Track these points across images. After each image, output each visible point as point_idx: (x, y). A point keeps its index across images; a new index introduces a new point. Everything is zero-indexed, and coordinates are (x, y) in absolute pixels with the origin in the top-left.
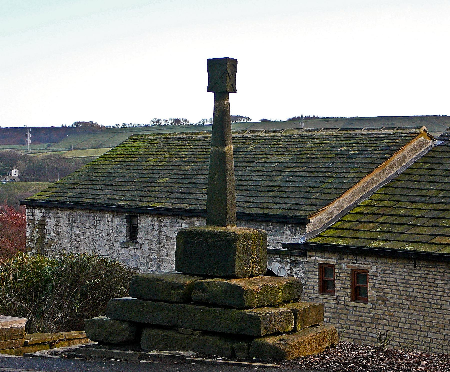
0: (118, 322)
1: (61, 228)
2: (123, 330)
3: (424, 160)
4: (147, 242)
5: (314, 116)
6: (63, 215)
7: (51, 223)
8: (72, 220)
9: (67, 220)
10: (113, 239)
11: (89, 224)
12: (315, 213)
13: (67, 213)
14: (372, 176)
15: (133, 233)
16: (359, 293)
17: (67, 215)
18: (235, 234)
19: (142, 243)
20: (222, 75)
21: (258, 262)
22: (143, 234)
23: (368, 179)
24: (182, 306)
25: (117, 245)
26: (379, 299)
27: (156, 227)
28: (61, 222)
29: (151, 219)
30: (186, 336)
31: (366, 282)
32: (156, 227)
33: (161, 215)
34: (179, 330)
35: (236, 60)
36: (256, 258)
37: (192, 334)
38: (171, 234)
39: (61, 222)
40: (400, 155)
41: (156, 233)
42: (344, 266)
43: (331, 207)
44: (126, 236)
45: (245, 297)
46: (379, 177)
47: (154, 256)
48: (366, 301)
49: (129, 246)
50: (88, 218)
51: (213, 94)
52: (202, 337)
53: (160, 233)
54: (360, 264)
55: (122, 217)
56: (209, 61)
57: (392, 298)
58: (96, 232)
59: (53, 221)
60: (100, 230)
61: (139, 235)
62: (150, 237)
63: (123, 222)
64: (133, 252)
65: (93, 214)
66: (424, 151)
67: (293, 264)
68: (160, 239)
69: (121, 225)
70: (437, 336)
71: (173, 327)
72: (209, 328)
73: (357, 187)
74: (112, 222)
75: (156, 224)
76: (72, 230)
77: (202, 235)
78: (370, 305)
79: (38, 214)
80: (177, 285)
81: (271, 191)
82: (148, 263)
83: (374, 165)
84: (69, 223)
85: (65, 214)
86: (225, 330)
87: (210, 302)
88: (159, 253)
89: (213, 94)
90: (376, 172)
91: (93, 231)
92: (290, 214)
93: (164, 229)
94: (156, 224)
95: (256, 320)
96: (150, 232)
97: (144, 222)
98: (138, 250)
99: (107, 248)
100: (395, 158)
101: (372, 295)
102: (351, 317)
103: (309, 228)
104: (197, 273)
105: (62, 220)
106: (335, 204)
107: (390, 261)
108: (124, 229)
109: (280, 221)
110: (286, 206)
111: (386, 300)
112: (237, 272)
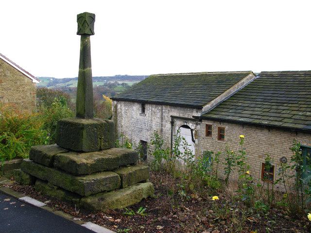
2: (28, 179)
3: (252, 84)
5: (78, 34)
6: (123, 103)
7: (119, 106)
12: (205, 104)
14: (230, 89)
15: (143, 111)
16: (221, 137)
18: (83, 125)
20: (86, 24)
23: (228, 91)
26: (228, 139)
31: (224, 133)
35: (94, 15)
40: (242, 81)
42: (215, 127)
43: (213, 102)
45: (78, 169)
46: (233, 90)
47: (150, 119)
48: (223, 140)
51: (80, 36)
52: (58, 191)
53: (152, 110)
54: (222, 126)
57: (233, 140)
59: (120, 105)
66: (252, 80)
67: (197, 124)
70: (251, 156)
73: (224, 94)
78: (225, 142)
79: (115, 102)
81: (258, 93)
88: (151, 118)
89: (80, 36)
90: (232, 88)
92: (196, 104)
93: (153, 109)
95: (83, 185)
97: (148, 107)
100: (240, 83)
101: (226, 138)
102: (218, 147)
103: (203, 110)
106: (214, 100)
107: (233, 125)
109: (192, 107)
110: (195, 101)
111: (231, 141)
112: (85, 148)
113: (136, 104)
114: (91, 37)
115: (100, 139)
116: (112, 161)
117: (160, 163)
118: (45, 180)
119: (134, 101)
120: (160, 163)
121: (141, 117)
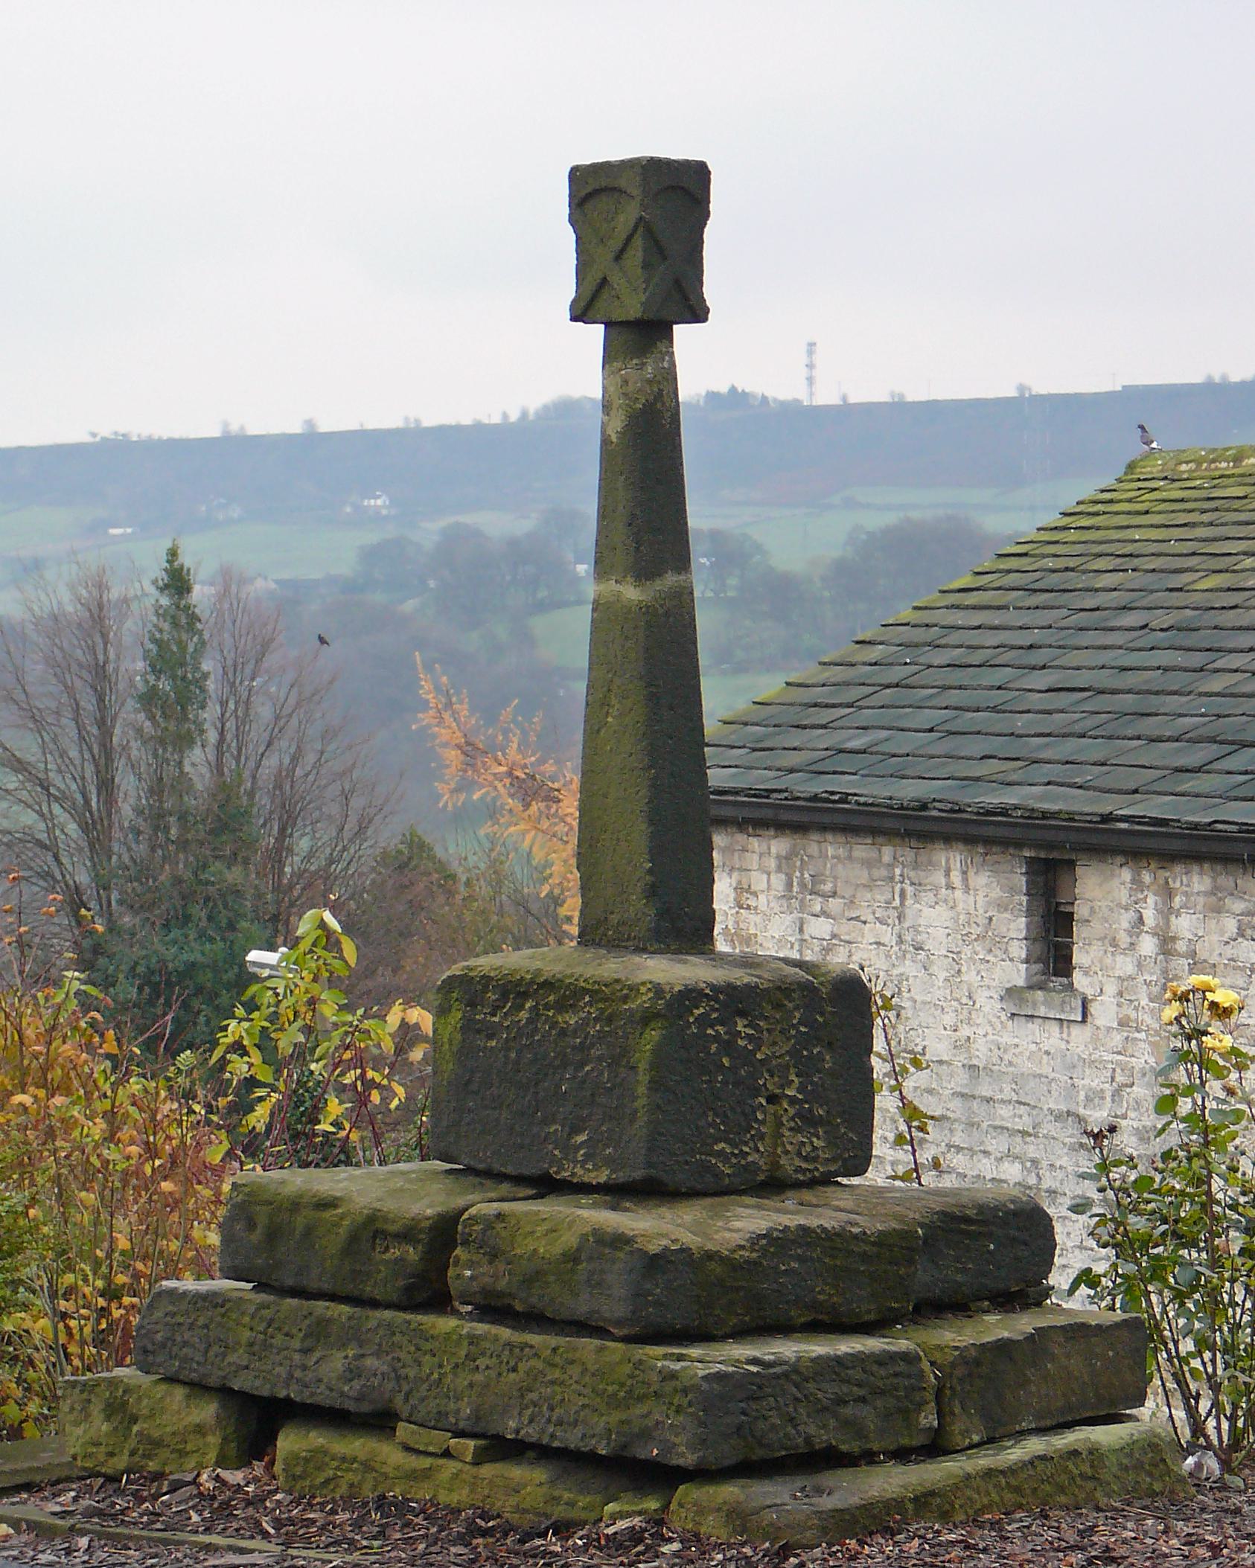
0: (180, 1392)
1: (758, 919)
2: (200, 1430)
4: (1111, 989)
5: (581, 313)
8: (803, 885)
9: (778, 881)
10: (970, 976)
11: (872, 902)
13: (779, 845)
17: (778, 857)
19: (1090, 992)
20: (643, 238)
21: (808, 1121)
22: (1096, 950)
24: (409, 1322)
25: (989, 1004)
27: (1150, 916)
28: (755, 894)
29: (1126, 874)
30: (426, 1462)
32: (1150, 916)
33: (1168, 858)
34: (403, 1430)
36: (793, 1101)
37: (447, 1454)
38: (1212, 951)
39: (755, 894)
41: (1148, 945)
44: (1027, 961)
49: (1035, 1004)
50: (865, 873)
51: (678, 330)
52: (487, 1470)
53: (1166, 943)
55: (1007, 867)
56: (579, 176)
58: (900, 941)
60: (915, 928)
61: (1077, 958)
62: (1125, 965)
63: (1012, 890)
64: (1052, 1037)
65: (887, 853)
68: (1165, 972)
69: (1002, 907)
71: (380, 1421)
72: (510, 1426)
74: (967, 889)
75: (1151, 900)
76: (801, 930)
77: (524, 995)
80: (392, 1228)
82: (1117, 1093)
83: (930, 682)
84: (788, 895)
85: (773, 850)
86: (571, 1439)
87: (519, 1307)
89: (600, 328)
91: (888, 936)
93: (1184, 925)
94: (1151, 900)
96: (1124, 939)
97: (1104, 894)
98: (1076, 1030)
99: (949, 1019)
104: (509, 1170)
105: (759, 881)
108: (1016, 926)
113: (952, 859)
114: (683, 333)
115: (772, 1099)
116: (865, 1257)
117: (1194, 1099)
118: (365, 1408)
119: (917, 827)
120: (1194, 1099)
121: (1034, 1045)
